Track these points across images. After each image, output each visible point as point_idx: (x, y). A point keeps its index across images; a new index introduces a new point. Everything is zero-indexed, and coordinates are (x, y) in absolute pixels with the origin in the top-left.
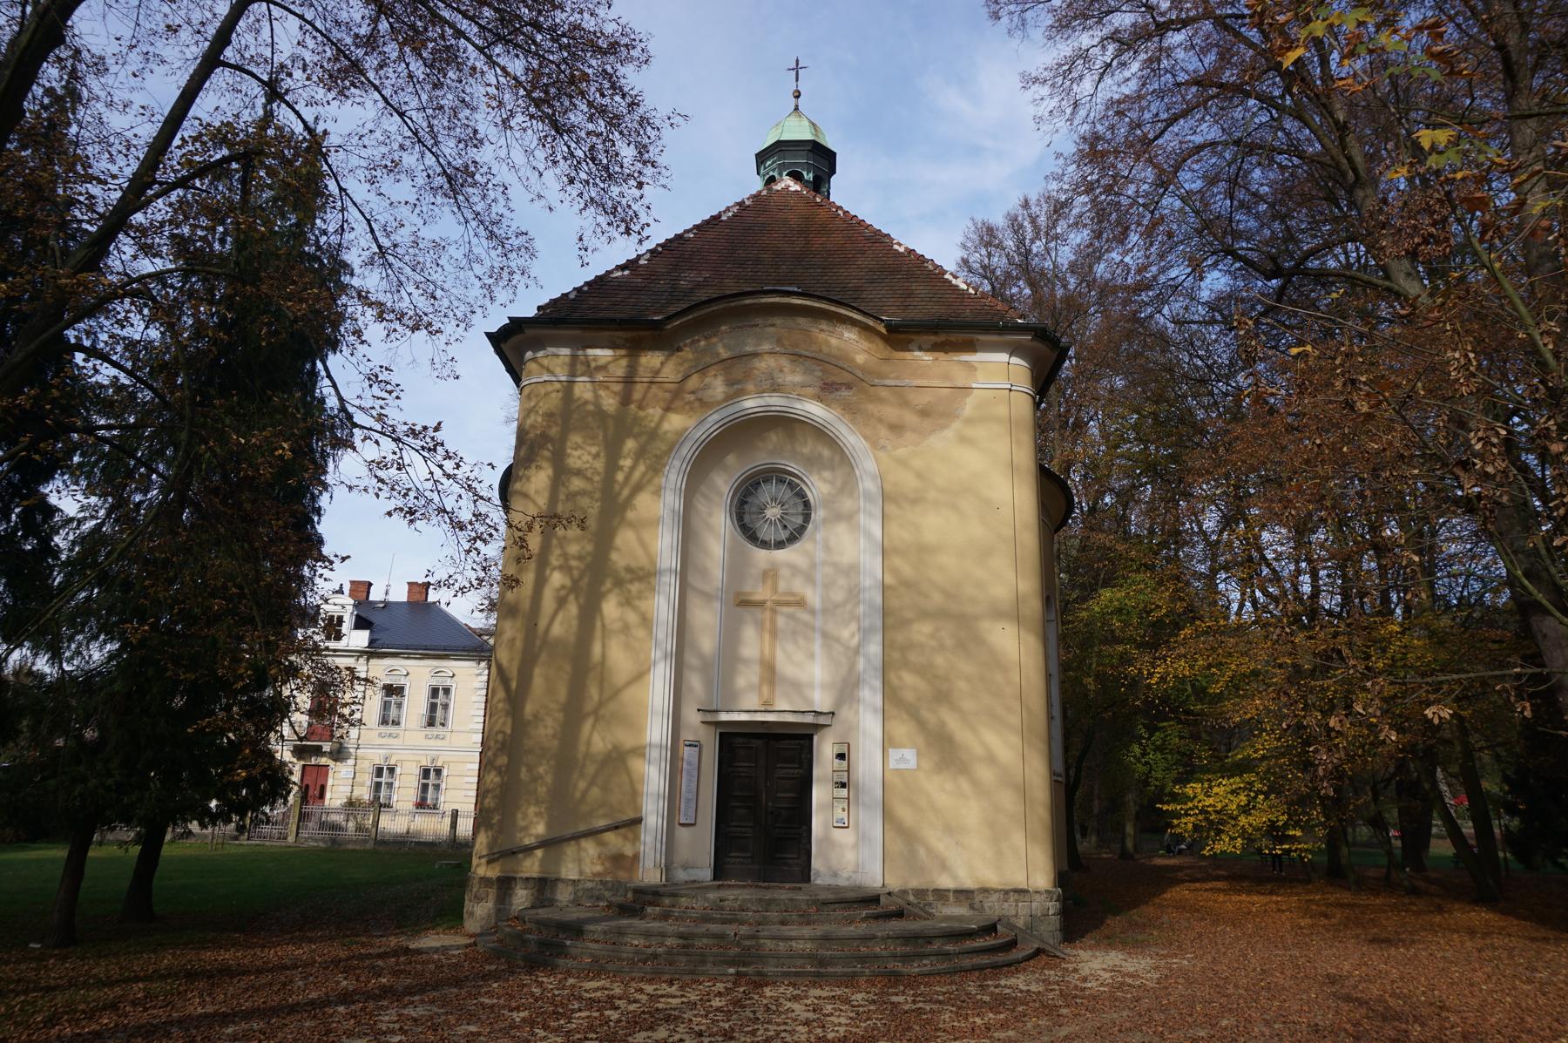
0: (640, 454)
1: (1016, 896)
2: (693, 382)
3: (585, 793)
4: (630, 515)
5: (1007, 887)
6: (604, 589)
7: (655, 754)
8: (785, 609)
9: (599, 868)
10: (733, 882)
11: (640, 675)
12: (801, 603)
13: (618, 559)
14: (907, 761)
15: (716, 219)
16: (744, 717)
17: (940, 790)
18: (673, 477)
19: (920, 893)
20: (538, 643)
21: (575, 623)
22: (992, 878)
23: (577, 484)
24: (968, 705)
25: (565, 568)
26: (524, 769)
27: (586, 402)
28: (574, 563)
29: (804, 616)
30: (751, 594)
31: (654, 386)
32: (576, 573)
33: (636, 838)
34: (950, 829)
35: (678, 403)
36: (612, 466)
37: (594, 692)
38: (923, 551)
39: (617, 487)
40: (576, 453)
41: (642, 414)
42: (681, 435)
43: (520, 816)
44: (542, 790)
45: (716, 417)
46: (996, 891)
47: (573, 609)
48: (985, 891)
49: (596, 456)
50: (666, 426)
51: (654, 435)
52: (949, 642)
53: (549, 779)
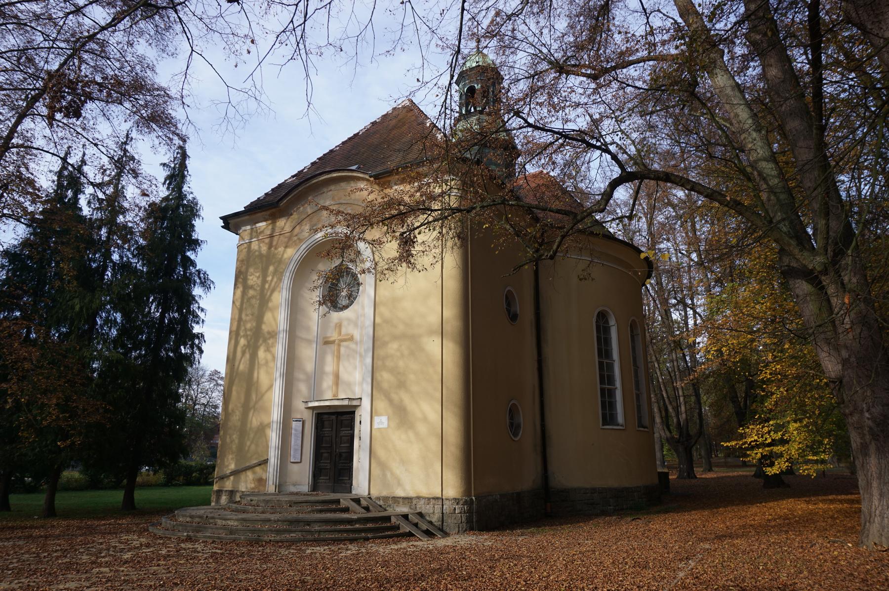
0: (275, 272)
1: (433, 501)
2: (297, 230)
3: (249, 447)
4: (270, 304)
5: (431, 496)
6: (259, 344)
8: (344, 344)
9: (253, 485)
10: (830, 497)
12: (351, 339)
13: (265, 328)
15: (356, 135)
17: (399, 439)
18: (286, 282)
19: (386, 499)
21: (248, 362)
22: (424, 491)
23: (251, 293)
24: (414, 388)
25: (246, 336)
26: (228, 437)
27: (256, 251)
28: (249, 333)
29: (353, 346)
31: (281, 236)
32: (249, 337)
33: (266, 471)
34: (404, 462)
35: (291, 242)
36: (264, 281)
37: (254, 397)
38: (395, 301)
40: (251, 278)
41: (276, 252)
44: (234, 447)
45: (304, 246)
46: (425, 498)
47: (247, 356)
48: (419, 498)
49: (258, 277)
50: (286, 256)
51: (280, 261)
52: (406, 352)
53: (237, 441)
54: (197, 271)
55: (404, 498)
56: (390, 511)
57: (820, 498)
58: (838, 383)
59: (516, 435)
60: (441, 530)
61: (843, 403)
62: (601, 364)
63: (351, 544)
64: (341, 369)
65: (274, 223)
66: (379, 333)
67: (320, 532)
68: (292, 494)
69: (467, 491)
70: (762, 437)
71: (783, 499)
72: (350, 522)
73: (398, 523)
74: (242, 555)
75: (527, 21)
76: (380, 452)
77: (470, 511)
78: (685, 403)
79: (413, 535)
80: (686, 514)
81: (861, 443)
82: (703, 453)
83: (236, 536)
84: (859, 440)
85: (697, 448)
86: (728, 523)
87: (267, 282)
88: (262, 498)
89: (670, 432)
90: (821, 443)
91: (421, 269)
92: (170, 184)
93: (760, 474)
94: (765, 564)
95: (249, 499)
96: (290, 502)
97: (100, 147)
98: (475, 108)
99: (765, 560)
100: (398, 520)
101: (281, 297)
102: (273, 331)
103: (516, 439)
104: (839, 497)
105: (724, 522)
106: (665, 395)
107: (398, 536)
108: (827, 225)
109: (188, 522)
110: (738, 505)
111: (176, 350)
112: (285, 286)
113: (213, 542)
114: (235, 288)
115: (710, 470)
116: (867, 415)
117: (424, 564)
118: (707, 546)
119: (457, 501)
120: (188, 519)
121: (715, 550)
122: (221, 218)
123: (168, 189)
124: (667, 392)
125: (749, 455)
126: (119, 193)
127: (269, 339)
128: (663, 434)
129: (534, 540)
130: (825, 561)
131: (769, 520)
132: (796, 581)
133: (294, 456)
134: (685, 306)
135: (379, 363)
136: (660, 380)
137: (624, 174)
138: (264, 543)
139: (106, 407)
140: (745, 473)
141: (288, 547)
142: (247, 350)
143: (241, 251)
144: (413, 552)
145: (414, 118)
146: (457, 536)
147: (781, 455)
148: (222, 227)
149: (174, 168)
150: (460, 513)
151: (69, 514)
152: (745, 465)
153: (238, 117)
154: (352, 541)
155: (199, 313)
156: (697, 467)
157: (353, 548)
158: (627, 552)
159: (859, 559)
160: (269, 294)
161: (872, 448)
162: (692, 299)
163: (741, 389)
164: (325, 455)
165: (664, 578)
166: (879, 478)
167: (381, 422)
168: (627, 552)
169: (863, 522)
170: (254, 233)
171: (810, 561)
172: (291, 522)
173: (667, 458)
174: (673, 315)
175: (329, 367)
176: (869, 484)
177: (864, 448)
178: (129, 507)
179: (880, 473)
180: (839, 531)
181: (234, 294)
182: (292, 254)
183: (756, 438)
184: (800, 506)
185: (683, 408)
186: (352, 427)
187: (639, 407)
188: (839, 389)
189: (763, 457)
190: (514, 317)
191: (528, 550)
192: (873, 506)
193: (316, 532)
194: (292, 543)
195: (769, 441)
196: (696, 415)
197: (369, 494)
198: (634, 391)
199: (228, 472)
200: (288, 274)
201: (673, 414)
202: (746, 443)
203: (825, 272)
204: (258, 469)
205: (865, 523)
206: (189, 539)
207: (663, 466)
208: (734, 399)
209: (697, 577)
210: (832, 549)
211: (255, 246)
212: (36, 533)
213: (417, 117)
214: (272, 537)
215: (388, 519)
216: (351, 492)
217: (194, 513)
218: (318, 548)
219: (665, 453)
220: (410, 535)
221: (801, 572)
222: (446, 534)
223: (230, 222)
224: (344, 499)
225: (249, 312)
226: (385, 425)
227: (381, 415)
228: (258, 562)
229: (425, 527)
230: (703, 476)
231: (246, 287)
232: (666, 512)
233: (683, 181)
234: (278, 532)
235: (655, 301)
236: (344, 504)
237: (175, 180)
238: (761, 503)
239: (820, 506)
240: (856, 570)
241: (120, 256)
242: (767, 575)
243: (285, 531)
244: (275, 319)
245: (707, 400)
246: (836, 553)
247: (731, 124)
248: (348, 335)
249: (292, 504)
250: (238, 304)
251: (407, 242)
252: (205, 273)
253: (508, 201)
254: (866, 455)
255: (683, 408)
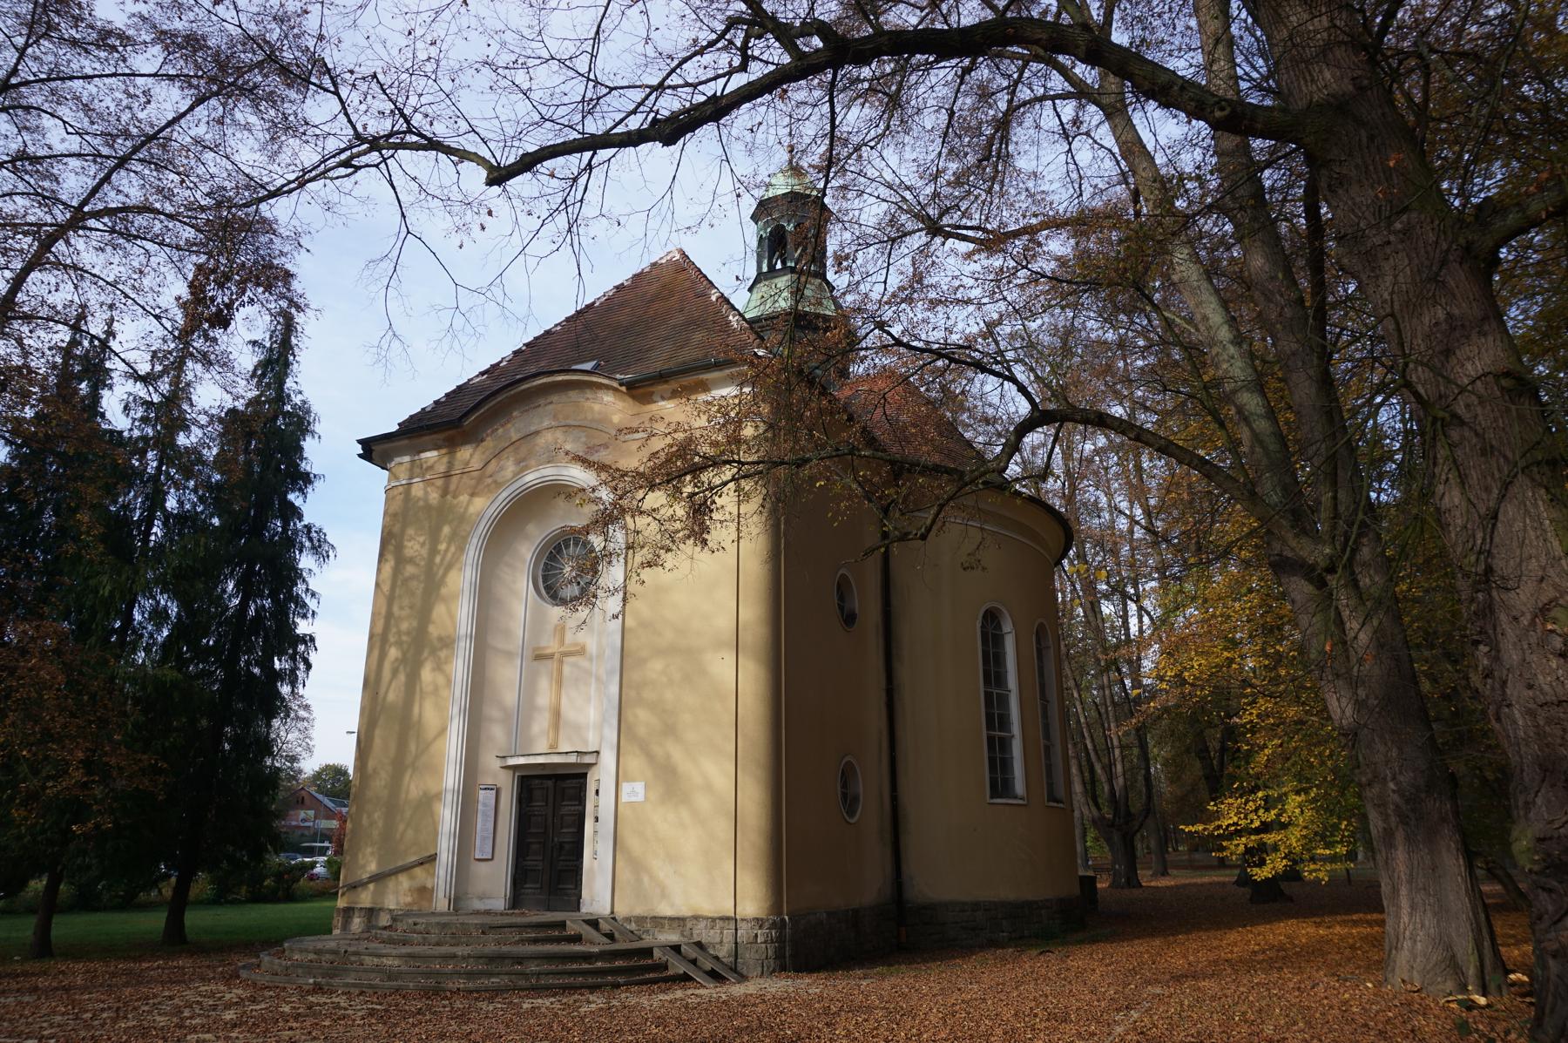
0: (453, 537)
2: (492, 466)
4: (444, 591)
5: (716, 915)
7: (449, 797)
9: (409, 899)
10: (1355, 917)
11: (443, 731)
12: (581, 651)
13: (433, 631)
14: (636, 794)
16: (540, 760)
17: (664, 821)
18: (471, 553)
19: (640, 920)
20: (379, 708)
21: (403, 688)
22: (707, 907)
23: (410, 570)
25: (399, 644)
26: (365, 816)
27: (419, 499)
28: (404, 638)
30: (544, 648)
31: (465, 476)
32: (405, 646)
35: (481, 487)
36: (433, 551)
37: (413, 747)
39: (435, 568)
40: (409, 544)
41: (455, 502)
42: (480, 515)
43: (360, 856)
44: (375, 833)
45: (504, 494)
46: (707, 918)
47: (402, 677)
48: (696, 918)
49: (423, 545)
50: (472, 510)
51: (462, 518)
53: (380, 824)
54: (305, 526)
55: (671, 919)
56: (648, 941)
57: (1339, 918)
58: (1351, 736)
59: (851, 813)
60: (734, 969)
61: (1359, 767)
62: (988, 696)
63: (591, 993)
64: (564, 701)
65: (452, 453)
66: (632, 644)
67: (539, 974)
68: (477, 913)
69: (776, 907)
70: (1246, 818)
71: (1279, 920)
72: (587, 957)
73: (664, 959)
74: (419, 1012)
75: (885, 154)
76: (632, 842)
77: (780, 939)
78: (1123, 758)
79: (690, 979)
80: (1125, 944)
81: (1385, 829)
82: (1153, 844)
83: (400, 983)
84: (1380, 824)
85: (1142, 836)
86: (1191, 958)
87: (439, 552)
88: (434, 920)
89: (1099, 809)
90: (1336, 827)
91: (715, 547)
92: (264, 375)
93: (1244, 880)
94: (1244, 1014)
95: (410, 921)
96: (482, 925)
97: (164, 321)
98: (784, 263)
99: (1244, 1008)
100: (664, 954)
101: (462, 580)
102: (449, 637)
103: (852, 821)
104: (1369, 917)
105: (1185, 957)
106: (1090, 746)
107: (666, 980)
108: (1335, 498)
109: (311, 961)
110: (1206, 930)
111: (266, 664)
112: (470, 561)
113: (362, 993)
114: (380, 561)
115: (1164, 873)
116: (1392, 785)
117: (722, 1021)
118: (1158, 991)
119: (759, 922)
120: (311, 956)
121: (1170, 996)
122: (359, 442)
123: (258, 385)
124: (1093, 741)
125: (1224, 849)
126: (179, 395)
127: (441, 649)
128: (1086, 812)
129: (886, 984)
130: (1331, 1007)
131: (1254, 952)
132: (1287, 1035)
133: (481, 849)
134: (1125, 597)
135: (631, 694)
136: (1082, 720)
137: (1036, 414)
138: (448, 994)
139: (157, 763)
140: (1221, 879)
141: (491, 1000)
142: (401, 668)
143: (393, 498)
144: (699, 1004)
145: (688, 284)
146: (761, 981)
147: (1275, 848)
148: (360, 456)
149: (271, 349)
150: (765, 942)
151: (78, 952)
152: (1222, 864)
153: (469, 329)
154: (593, 988)
155: (308, 600)
156: (1142, 869)
157: (597, 1001)
158: (1035, 999)
159: (1378, 1003)
160: (441, 572)
161: (1400, 836)
162: (1135, 586)
163: (1214, 738)
164: (534, 847)
165: (1094, 1034)
166: (1410, 882)
167: (634, 791)
168: (1035, 999)
169: (1387, 948)
170: (416, 469)
171: (1309, 1008)
172: (492, 959)
173: (1093, 854)
174: (1103, 608)
175: (544, 698)
176: (1395, 891)
177: (1389, 834)
178: (175, 939)
179: (1411, 875)
180: (1359, 967)
181: (379, 570)
182: (483, 508)
183: (1235, 819)
184: (1305, 931)
185: (1119, 767)
186: (580, 798)
187: (1049, 768)
188: (1353, 746)
189: (1248, 851)
190: (849, 619)
191: (881, 998)
192: (1402, 925)
193: (533, 974)
194: (494, 993)
195: (1257, 824)
196: (1140, 778)
197: (612, 912)
198: (1042, 742)
199: (365, 876)
200: (475, 540)
201: (1103, 778)
202: (1219, 827)
203: (1331, 570)
204: (418, 871)
205: (1390, 950)
206: (318, 989)
207: (1087, 867)
208: (1203, 753)
209: (1142, 1033)
210: (1342, 991)
211: (417, 490)
212: (42, 982)
213: (693, 282)
214: (461, 983)
215: (648, 952)
216: (578, 909)
217: (320, 946)
218: (540, 1001)
219: (1088, 844)
220: (686, 978)
221: (1295, 1023)
222: (743, 978)
223: (374, 449)
224: (573, 921)
225: (406, 602)
226: (640, 798)
227: (634, 780)
228: (453, 1022)
229: (708, 966)
230: (1153, 884)
231: (401, 561)
232: (1094, 940)
233: (1124, 425)
234: (470, 975)
235: (1073, 584)
236: (572, 928)
237: (272, 370)
238: (1245, 926)
239: (1336, 930)
240: (1372, 1019)
241: (178, 501)
242: (1245, 1029)
243: (481, 974)
244: (452, 617)
245: (1160, 754)
246: (1347, 996)
247: (1197, 330)
248: (576, 644)
249: (486, 929)
250: (386, 588)
251: (700, 511)
252: (319, 531)
253: (859, 450)
254: (1390, 845)
255: (1119, 767)
